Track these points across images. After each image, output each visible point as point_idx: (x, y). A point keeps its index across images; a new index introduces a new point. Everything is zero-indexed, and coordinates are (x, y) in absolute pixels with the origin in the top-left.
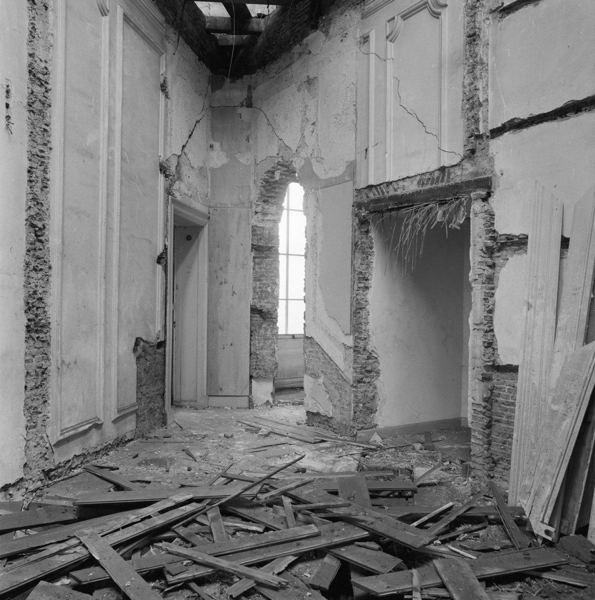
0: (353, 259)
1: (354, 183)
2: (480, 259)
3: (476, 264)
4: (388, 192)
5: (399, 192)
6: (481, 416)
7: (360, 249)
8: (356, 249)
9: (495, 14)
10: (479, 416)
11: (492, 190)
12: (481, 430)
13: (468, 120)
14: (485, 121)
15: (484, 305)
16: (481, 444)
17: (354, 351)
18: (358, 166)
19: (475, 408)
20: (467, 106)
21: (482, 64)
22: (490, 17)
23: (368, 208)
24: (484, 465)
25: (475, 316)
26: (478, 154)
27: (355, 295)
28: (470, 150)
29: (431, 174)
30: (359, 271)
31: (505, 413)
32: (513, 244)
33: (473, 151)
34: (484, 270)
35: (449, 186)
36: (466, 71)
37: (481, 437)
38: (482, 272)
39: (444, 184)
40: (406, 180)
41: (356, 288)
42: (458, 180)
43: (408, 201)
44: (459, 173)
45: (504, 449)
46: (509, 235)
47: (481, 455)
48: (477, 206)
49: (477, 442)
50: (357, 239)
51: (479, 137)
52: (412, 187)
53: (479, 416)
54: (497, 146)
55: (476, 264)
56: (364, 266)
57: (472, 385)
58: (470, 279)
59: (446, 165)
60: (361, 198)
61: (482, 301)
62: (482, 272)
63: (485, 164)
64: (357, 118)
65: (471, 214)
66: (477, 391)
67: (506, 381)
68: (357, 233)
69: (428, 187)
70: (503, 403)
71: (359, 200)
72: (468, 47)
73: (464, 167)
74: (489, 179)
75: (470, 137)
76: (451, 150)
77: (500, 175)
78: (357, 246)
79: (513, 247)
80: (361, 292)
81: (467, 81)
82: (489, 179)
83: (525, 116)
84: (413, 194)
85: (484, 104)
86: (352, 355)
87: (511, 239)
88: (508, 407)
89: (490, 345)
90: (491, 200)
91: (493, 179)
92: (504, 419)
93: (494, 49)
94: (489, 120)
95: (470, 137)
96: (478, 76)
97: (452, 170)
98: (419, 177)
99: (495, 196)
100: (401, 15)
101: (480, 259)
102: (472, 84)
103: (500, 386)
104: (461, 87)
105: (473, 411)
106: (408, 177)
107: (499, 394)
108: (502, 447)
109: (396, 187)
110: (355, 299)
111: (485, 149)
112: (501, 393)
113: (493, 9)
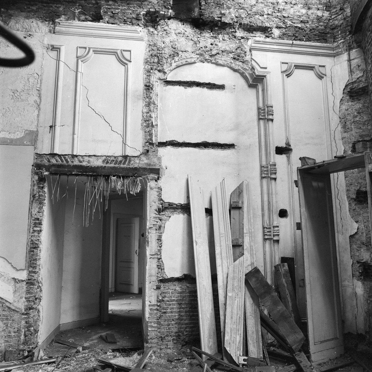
0: (31, 208)
1: (35, 148)
2: (154, 215)
3: (152, 218)
4: (73, 162)
5: (84, 164)
6: (155, 312)
7: (36, 199)
8: (33, 199)
9: (162, 81)
10: (154, 312)
11: (160, 176)
12: (156, 321)
13: (145, 132)
14: (156, 136)
15: (158, 243)
16: (156, 329)
17: (27, 283)
18: (39, 135)
19: (151, 308)
20: (145, 124)
21: (154, 104)
22: (159, 81)
23: (49, 170)
24: (158, 343)
25: (151, 250)
26: (150, 153)
27: (30, 237)
28: (147, 150)
29: (115, 158)
30: (36, 217)
31: (169, 307)
32: (171, 208)
33: (148, 151)
34: (157, 222)
35: (130, 168)
36: (144, 105)
37: (156, 325)
38: (156, 223)
39: (125, 166)
40: (91, 157)
41: (31, 230)
42: (136, 166)
43: (93, 172)
44: (138, 162)
45: (169, 329)
46: (171, 203)
47: (156, 337)
48: (152, 184)
49: (153, 329)
50: (35, 192)
51: (152, 144)
52: (98, 163)
53: (154, 312)
54: (163, 151)
55: (152, 218)
56: (40, 214)
57: (149, 293)
58: (147, 227)
59: (129, 155)
60: (41, 161)
61: (156, 241)
62: (156, 223)
63: (155, 160)
64: (40, 100)
65: (148, 188)
66: (153, 297)
67: (170, 287)
68: (36, 188)
69: (112, 165)
70: (168, 301)
71: (39, 162)
72: (145, 91)
73: (141, 159)
74: (159, 170)
75: (146, 143)
76: (135, 146)
77: (165, 168)
78: (35, 197)
79: (171, 210)
80: (36, 234)
81: (145, 110)
82: (159, 170)
83: (181, 141)
84: (98, 167)
85: (155, 126)
86: (25, 287)
87: (172, 205)
88: (171, 303)
89: (160, 267)
90: (158, 181)
91: (161, 170)
92: (169, 310)
93: (161, 99)
94: (158, 136)
95: (146, 143)
96: (152, 110)
97: (132, 159)
98: (104, 158)
99: (162, 180)
100: (93, 49)
101: (154, 215)
102: (148, 113)
103: (166, 291)
104: (141, 112)
105: (149, 310)
106: (94, 156)
107: (165, 296)
108: (168, 328)
109: (82, 160)
110: (30, 240)
111: (156, 152)
112: (167, 295)
113: (161, 78)
